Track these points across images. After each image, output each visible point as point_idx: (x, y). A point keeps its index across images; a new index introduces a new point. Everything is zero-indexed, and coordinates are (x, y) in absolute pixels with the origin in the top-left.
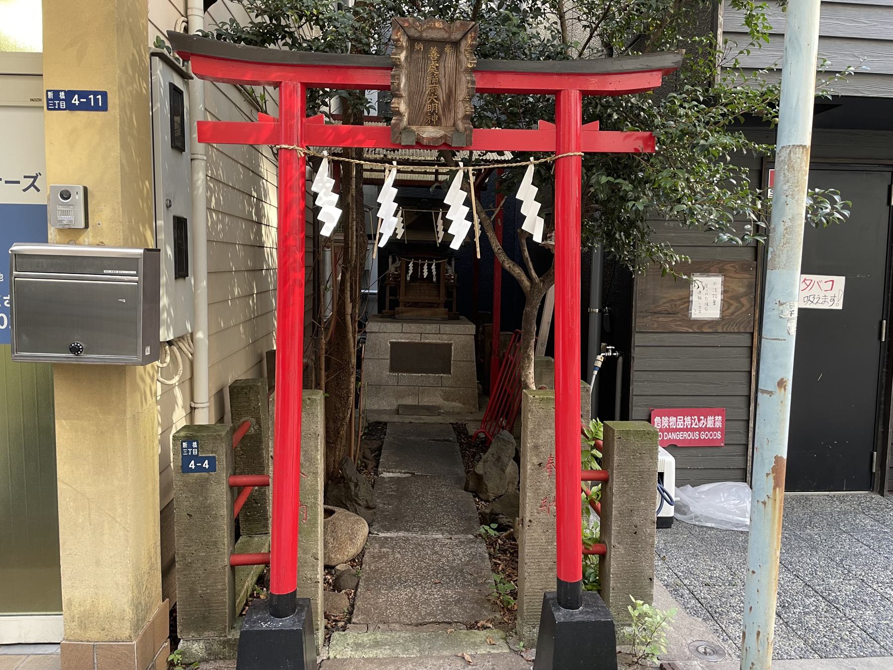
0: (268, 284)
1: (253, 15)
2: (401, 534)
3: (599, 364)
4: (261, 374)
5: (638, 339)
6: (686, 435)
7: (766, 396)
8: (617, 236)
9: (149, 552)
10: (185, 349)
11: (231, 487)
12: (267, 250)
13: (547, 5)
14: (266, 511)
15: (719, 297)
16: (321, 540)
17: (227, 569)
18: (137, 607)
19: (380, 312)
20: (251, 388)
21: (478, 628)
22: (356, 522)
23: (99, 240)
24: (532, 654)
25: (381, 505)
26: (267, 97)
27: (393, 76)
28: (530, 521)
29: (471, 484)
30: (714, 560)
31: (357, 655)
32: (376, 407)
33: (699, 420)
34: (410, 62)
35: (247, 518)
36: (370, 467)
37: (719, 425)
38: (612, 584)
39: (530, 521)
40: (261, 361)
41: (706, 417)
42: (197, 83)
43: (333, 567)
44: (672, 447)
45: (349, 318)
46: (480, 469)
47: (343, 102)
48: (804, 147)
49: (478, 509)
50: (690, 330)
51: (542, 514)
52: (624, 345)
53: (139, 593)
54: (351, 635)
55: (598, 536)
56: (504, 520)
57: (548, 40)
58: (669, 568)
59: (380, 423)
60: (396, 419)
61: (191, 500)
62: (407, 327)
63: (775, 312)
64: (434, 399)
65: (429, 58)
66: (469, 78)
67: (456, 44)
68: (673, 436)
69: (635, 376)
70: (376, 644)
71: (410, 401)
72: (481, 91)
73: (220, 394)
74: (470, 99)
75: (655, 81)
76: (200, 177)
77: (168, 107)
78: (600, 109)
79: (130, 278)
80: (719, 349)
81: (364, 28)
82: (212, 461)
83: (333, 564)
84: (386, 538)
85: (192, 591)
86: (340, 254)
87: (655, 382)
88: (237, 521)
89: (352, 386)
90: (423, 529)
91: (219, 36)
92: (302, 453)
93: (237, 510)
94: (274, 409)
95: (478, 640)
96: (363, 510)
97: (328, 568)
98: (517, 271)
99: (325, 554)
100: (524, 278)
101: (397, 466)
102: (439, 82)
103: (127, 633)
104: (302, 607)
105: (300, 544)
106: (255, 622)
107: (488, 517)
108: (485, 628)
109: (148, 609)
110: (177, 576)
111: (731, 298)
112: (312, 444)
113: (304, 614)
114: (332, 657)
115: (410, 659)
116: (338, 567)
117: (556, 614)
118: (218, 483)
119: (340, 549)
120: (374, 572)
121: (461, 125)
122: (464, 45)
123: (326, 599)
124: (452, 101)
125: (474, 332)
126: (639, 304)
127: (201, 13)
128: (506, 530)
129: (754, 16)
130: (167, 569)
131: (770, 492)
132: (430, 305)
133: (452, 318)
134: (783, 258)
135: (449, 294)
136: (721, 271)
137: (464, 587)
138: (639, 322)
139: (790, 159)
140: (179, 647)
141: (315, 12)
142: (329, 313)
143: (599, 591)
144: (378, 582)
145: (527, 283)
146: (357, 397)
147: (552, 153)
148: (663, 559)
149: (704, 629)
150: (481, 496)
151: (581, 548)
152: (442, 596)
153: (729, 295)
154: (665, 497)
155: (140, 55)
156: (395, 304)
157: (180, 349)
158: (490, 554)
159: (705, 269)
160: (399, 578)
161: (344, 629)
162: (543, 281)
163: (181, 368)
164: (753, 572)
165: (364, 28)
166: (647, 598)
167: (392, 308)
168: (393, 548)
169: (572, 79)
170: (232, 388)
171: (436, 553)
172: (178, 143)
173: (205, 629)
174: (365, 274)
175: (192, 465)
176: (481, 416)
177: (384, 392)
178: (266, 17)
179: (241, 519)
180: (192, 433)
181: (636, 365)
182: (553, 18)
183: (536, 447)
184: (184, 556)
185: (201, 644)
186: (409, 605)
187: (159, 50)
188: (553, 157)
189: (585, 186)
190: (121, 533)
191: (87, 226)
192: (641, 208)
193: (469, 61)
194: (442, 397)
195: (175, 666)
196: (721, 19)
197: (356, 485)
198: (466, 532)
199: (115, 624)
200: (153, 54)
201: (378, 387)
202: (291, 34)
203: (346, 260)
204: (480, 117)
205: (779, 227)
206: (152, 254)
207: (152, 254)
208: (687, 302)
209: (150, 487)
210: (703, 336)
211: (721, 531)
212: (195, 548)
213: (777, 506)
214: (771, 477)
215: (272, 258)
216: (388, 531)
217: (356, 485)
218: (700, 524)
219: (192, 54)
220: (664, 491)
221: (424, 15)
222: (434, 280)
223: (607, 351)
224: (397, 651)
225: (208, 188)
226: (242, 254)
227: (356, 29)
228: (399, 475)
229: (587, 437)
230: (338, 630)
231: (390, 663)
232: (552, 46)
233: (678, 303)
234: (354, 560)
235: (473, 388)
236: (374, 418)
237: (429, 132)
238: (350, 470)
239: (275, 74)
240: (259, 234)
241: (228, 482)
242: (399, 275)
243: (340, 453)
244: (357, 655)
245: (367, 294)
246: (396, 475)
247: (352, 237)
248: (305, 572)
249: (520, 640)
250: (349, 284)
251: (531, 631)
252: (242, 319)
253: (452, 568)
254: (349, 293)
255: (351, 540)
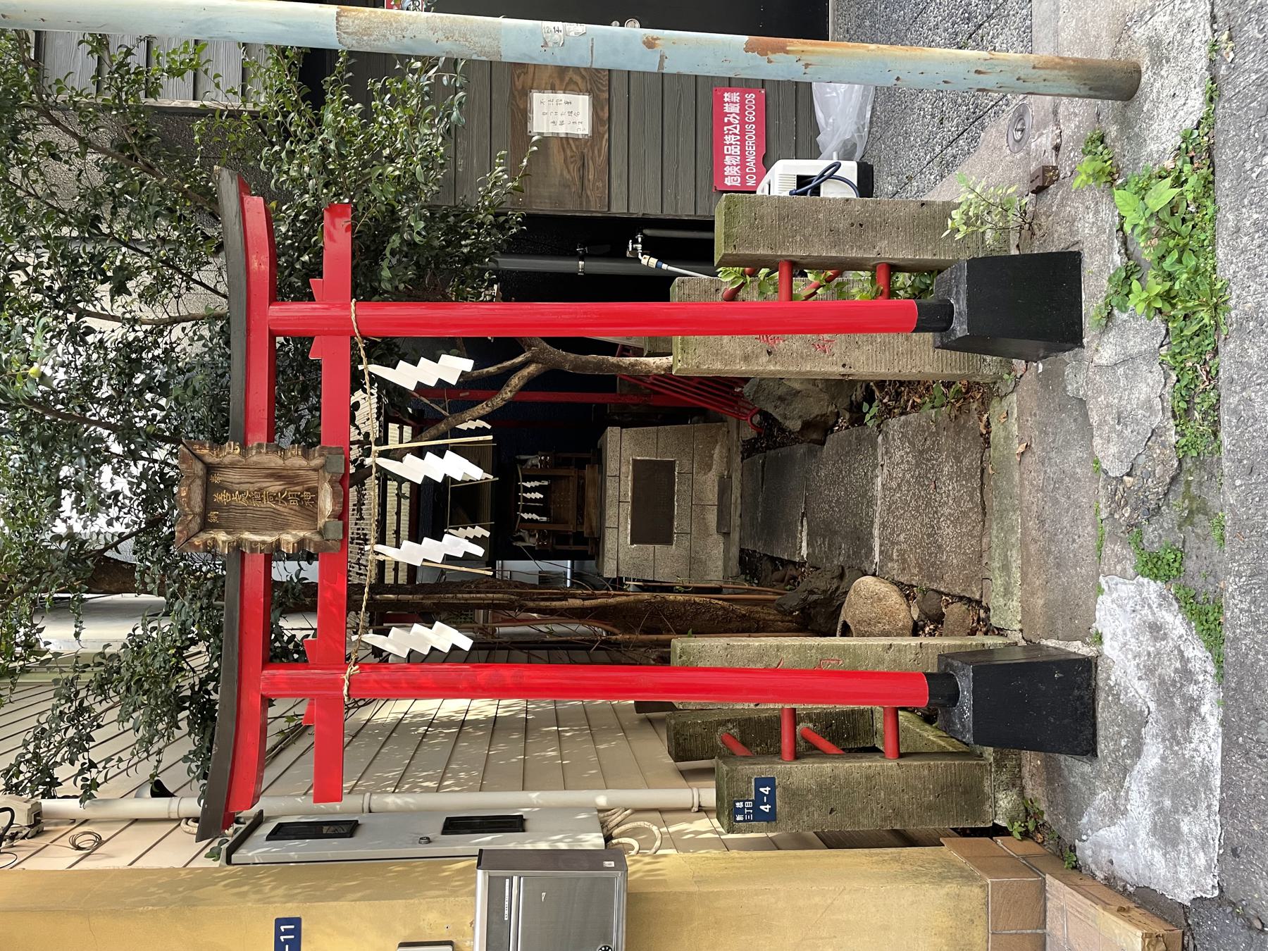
0: (546, 712)
1: (177, 733)
2: (876, 532)
3: (653, 261)
4: (662, 720)
5: (618, 209)
6: (750, 143)
7: (666, 63)
8: (465, 250)
9: (877, 863)
10: (619, 819)
11: (797, 756)
12: (501, 713)
13: (160, 340)
14: (843, 713)
15: (561, 96)
16: (880, 638)
17: (902, 762)
18: (944, 878)
19: (592, 558)
20: (677, 733)
21: (988, 433)
22: (857, 593)
23: (467, 928)
24: (1019, 364)
25: (841, 559)
26: (290, 713)
27: (253, 550)
28: (844, 366)
29: (815, 436)
30: (912, 110)
31: (1018, 592)
32: (720, 563)
33: (730, 123)
34: (235, 529)
35: (848, 736)
36: (794, 573)
37: (736, 97)
38: (928, 257)
39: (844, 366)
40: (650, 720)
41: (726, 114)
42: (264, 804)
43: (915, 623)
44: (766, 162)
45: (587, 603)
46: (795, 425)
47: (287, 611)
48: (339, 15)
49: (847, 428)
50: (606, 136)
51: (834, 350)
52: (627, 227)
53: (926, 875)
54: (995, 600)
55: (869, 273)
56: (859, 394)
57: (204, 345)
58: (921, 172)
59: (741, 558)
60: (735, 536)
61: (811, 809)
62: (610, 522)
63: (557, 51)
64: (709, 485)
65: (229, 504)
66: (254, 452)
67: (210, 469)
68: (751, 160)
69: (669, 213)
70: (1006, 567)
71: (712, 517)
72: (272, 432)
73: (687, 775)
74: (282, 449)
75: (255, 204)
76: (392, 801)
77: (297, 842)
78: (293, 276)
79: (515, 887)
80: (632, 97)
81: (193, 586)
82: (761, 782)
83: (911, 623)
84: (881, 552)
85: (930, 808)
86: (503, 614)
87: (677, 185)
88: (850, 751)
89: (680, 598)
90: (871, 502)
91: (205, 776)
92: (752, 666)
93: (835, 750)
94: (693, 703)
95: (1002, 434)
96: (844, 584)
97: (916, 630)
98: (516, 381)
99: (898, 635)
100: (525, 372)
101: (793, 536)
102: (260, 490)
103: (977, 890)
104: (947, 665)
105: (870, 669)
106: (963, 726)
107: (855, 416)
108: (988, 425)
109: (949, 864)
110: (912, 827)
111: (562, 80)
112: (739, 653)
113: (956, 663)
114: (1018, 626)
115: (1023, 524)
116: (915, 617)
117: (959, 334)
118: (790, 774)
119: (891, 614)
120: (921, 569)
121: (317, 462)
122: (211, 458)
123: (952, 634)
124: (285, 473)
125: (617, 430)
126: (571, 207)
127: (175, 801)
128: (873, 392)
129: (170, 67)
130: (906, 839)
131: (793, 57)
132: (581, 489)
133: (598, 459)
134: (485, 41)
135: (566, 463)
136: (525, 94)
137: (939, 451)
138: (595, 208)
139: (355, 33)
140: (1004, 825)
141: (172, 651)
142: (579, 628)
143: (940, 272)
144: (933, 564)
145: (532, 368)
146: (698, 590)
147: (352, 338)
148: (910, 178)
149: (994, 130)
150: (831, 423)
151: (882, 301)
152: (951, 479)
153: (557, 83)
154: (830, 174)
155: (224, 878)
156: (579, 538)
157: (618, 825)
158: (901, 414)
159: (522, 116)
160: (929, 536)
161: (987, 610)
162: (530, 347)
163: (641, 824)
164: (898, 79)
165: (193, 586)
166: (946, 209)
167: (585, 541)
168: (893, 543)
169: (255, 316)
170: (677, 758)
171: (899, 485)
172: (348, 829)
173: (981, 791)
174: (545, 579)
175: (766, 808)
176: (732, 421)
177: (701, 553)
178: (180, 716)
179: (852, 746)
180: (726, 810)
181: (653, 211)
182: (177, 331)
183: (746, 358)
184: (885, 819)
185: (1000, 795)
186: (961, 524)
187: (223, 854)
188: (358, 339)
189: (398, 296)
190: (847, 897)
191: (450, 943)
192: (422, 224)
193: (231, 452)
194: (706, 475)
195: (1027, 830)
196: (177, 103)
197: (811, 592)
198: (874, 446)
199: (965, 905)
200: (229, 862)
201: (693, 561)
202: (203, 682)
203: (510, 606)
204: (307, 434)
205: (443, 47)
206: (483, 859)
207: (483, 859)
208: (567, 141)
209: (793, 862)
210: (614, 118)
211: (876, 97)
212: (874, 805)
213: (810, 48)
214: (772, 57)
215: (510, 706)
216: (872, 549)
217: (811, 592)
218: (867, 125)
219: (227, 809)
220: (822, 175)
221: (172, 508)
222: (546, 483)
223: (635, 249)
224: (1013, 540)
225: (410, 791)
226: (502, 747)
227: (194, 596)
228: (804, 534)
229: (743, 284)
230: (988, 618)
231: (1028, 550)
232: (211, 340)
233: (569, 153)
234: (907, 596)
235: (696, 429)
236: (734, 563)
237: (327, 504)
238: (793, 599)
239: (252, 700)
240: (475, 723)
241: (788, 762)
242: (539, 532)
243: (770, 614)
244: (1018, 592)
245: (572, 572)
246: (805, 539)
247: (480, 599)
248: (908, 663)
249: (1001, 378)
250: (542, 603)
251: (989, 366)
252: (590, 746)
253: (918, 465)
254: (554, 603)
255: (880, 600)
